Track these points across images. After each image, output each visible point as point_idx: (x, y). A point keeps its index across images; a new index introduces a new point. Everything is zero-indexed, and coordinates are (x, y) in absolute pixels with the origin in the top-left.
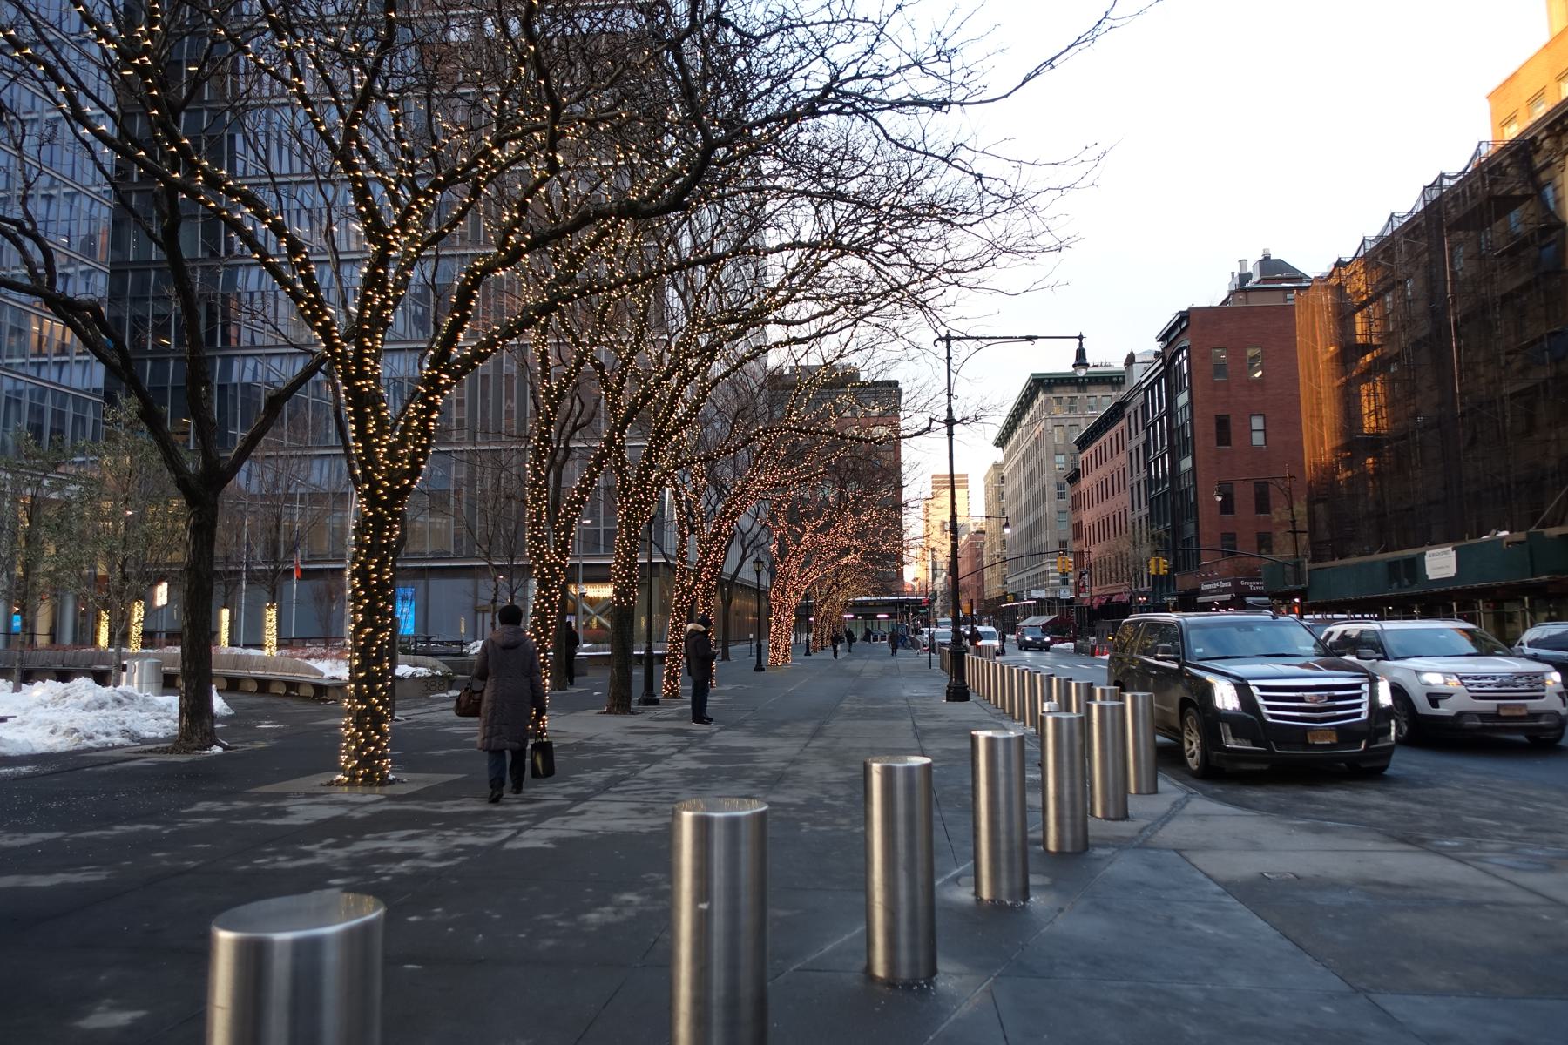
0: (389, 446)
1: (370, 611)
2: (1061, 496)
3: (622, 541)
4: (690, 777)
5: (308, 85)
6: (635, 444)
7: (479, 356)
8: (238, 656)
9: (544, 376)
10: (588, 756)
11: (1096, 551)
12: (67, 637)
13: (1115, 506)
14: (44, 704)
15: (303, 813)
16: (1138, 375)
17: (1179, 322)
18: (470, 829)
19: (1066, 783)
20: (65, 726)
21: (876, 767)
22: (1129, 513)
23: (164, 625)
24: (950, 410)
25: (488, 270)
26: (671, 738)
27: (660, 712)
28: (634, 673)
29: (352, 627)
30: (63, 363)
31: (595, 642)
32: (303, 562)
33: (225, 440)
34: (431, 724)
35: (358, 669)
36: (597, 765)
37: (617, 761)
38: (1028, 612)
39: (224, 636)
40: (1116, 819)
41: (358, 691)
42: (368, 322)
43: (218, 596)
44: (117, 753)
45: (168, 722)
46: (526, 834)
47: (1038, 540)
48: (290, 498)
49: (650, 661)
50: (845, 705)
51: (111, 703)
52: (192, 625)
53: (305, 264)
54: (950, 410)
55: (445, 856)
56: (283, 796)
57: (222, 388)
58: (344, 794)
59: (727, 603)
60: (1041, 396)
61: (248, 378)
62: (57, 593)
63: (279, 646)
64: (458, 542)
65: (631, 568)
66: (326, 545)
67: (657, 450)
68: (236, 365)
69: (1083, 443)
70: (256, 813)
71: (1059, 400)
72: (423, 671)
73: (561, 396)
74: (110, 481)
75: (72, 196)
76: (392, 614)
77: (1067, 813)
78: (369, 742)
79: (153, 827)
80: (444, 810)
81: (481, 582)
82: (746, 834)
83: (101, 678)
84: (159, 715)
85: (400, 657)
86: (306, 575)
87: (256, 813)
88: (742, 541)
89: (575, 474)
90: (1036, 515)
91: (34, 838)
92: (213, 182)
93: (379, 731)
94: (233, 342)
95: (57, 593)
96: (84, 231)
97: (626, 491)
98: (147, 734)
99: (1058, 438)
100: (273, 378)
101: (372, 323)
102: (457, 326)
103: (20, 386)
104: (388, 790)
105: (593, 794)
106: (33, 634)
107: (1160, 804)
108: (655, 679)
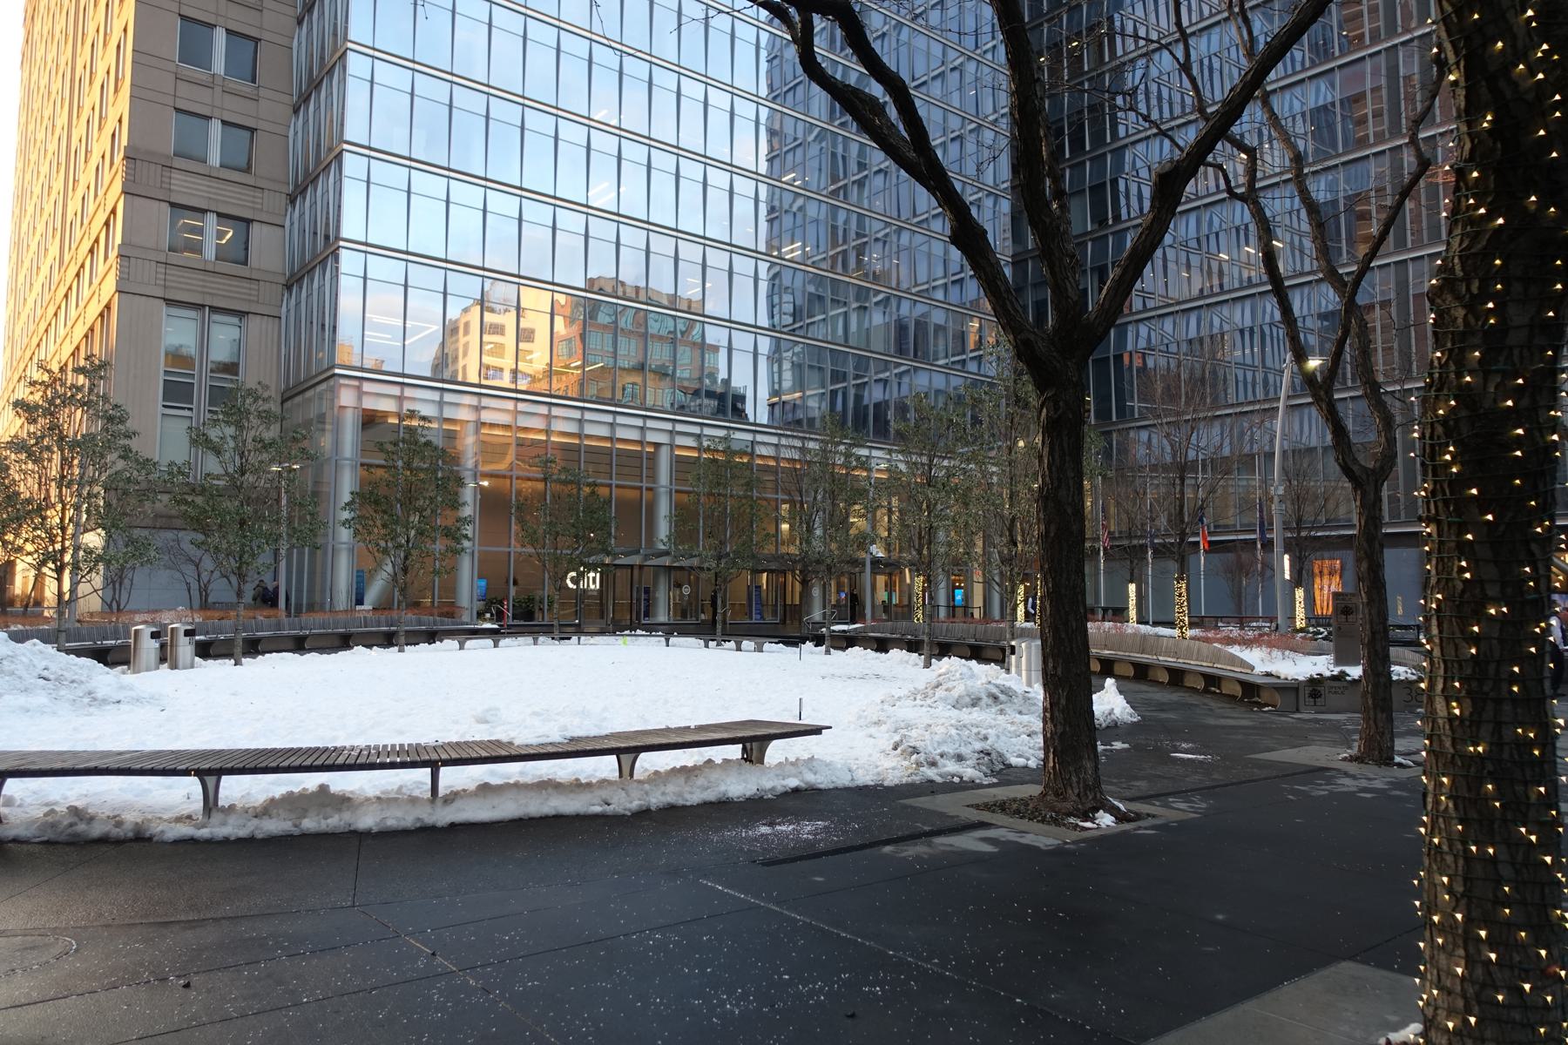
8: (1145, 637)
30: (980, 357)
35: (1465, 729)
51: (985, 700)
86: (1214, 547)
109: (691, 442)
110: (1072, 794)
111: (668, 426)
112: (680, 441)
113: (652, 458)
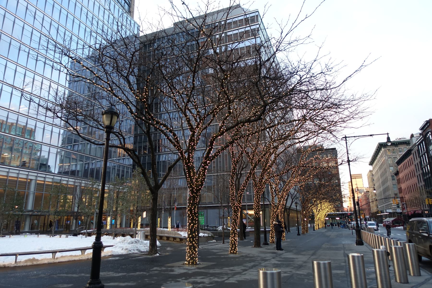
0: (196, 179)
1: (193, 220)
2: (393, 179)
3: (256, 199)
4: (275, 266)
5: (177, 98)
6: (258, 171)
7: (216, 155)
8: (162, 231)
9: (233, 157)
10: (248, 259)
11: (407, 197)
12: (124, 226)
13: (412, 182)
14: (120, 242)
15: (178, 271)
16: (414, 141)
17: (426, 124)
18: (216, 277)
19: (383, 270)
20: (125, 248)
21: (315, 262)
22: (418, 184)
23: (145, 223)
24: (348, 158)
25: (217, 137)
26: (271, 254)
27: (269, 247)
28: (261, 236)
29: (188, 224)
31: (252, 227)
32: (177, 206)
33: (159, 175)
34: (208, 249)
35: (190, 234)
36: (250, 261)
37: (255, 261)
38: (386, 216)
39: (159, 225)
40: (404, 283)
41: (190, 240)
42: (190, 150)
43: (158, 216)
44: (136, 255)
45: (147, 247)
46: (231, 279)
47: (387, 194)
48: (174, 189)
49: (265, 232)
50: (324, 246)
52: (152, 223)
53: (177, 138)
54: (348, 158)
55: (210, 283)
56: (173, 267)
57: (158, 162)
58: (187, 267)
59: (289, 215)
60: (383, 149)
61: (164, 160)
62: (121, 215)
63: (171, 228)
64: (214, 199)
65: (259, 206)
66: (182, 202)
67: (264, 174)
68: (161, 156)
69: (399, 163)
70: (167, 271)
71: (389, 150)
72: (206, 235)
73: (237, 162)
74: (134, 187)
75: (126, 120)
76: (198, 220)
77: (384, 280)
78: (193, 253)
79: (145, 273)
80: (211, 272)
81: (221, 210)
82: (276, 277)
83: (132, 236)
84: (144, 246)
85: (200, 231)
86: (177, 209)
87: (167, 271)
88: (292, 197)
89: (243, 181)
90: (385, 186)
91: (120, 274)
92: (158, 123)
93: (195, 251)
94: (161, 151)
95: (121, 215)
96: (129, 127)
97: (256, 185)
98: (142, 250)
99: (390, 161)
100: (169, 159)
101: (191, 149)
102: (210, 150)
103: (115, 165)
104: (197, 266)
105: (248, 269)
106: (116, 225)
107: (420, 280)
108: (267, 238)
109: (42, 179)
110: (153, 252)
111: (36, 174)
112: (39, 179)
113: (30, 183)
